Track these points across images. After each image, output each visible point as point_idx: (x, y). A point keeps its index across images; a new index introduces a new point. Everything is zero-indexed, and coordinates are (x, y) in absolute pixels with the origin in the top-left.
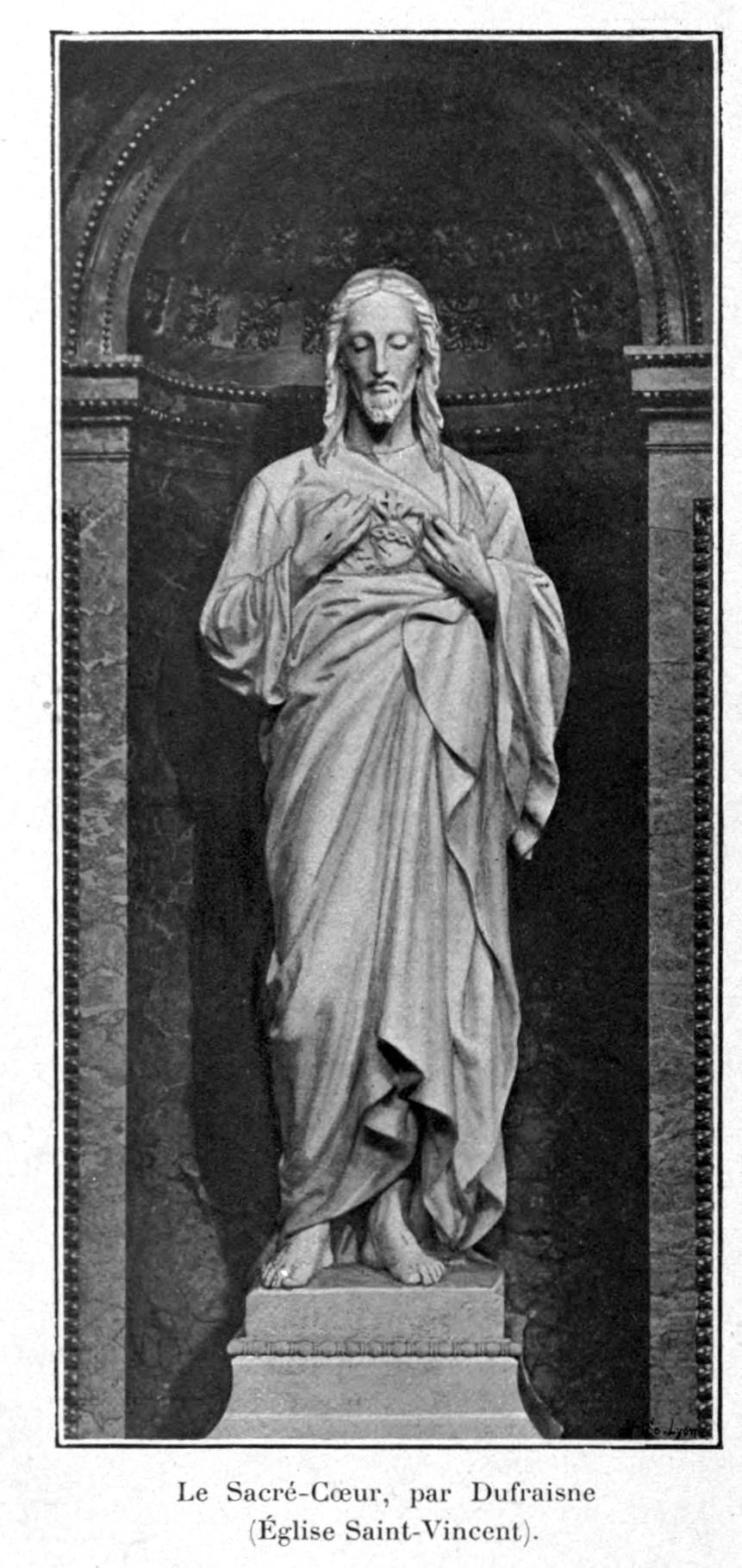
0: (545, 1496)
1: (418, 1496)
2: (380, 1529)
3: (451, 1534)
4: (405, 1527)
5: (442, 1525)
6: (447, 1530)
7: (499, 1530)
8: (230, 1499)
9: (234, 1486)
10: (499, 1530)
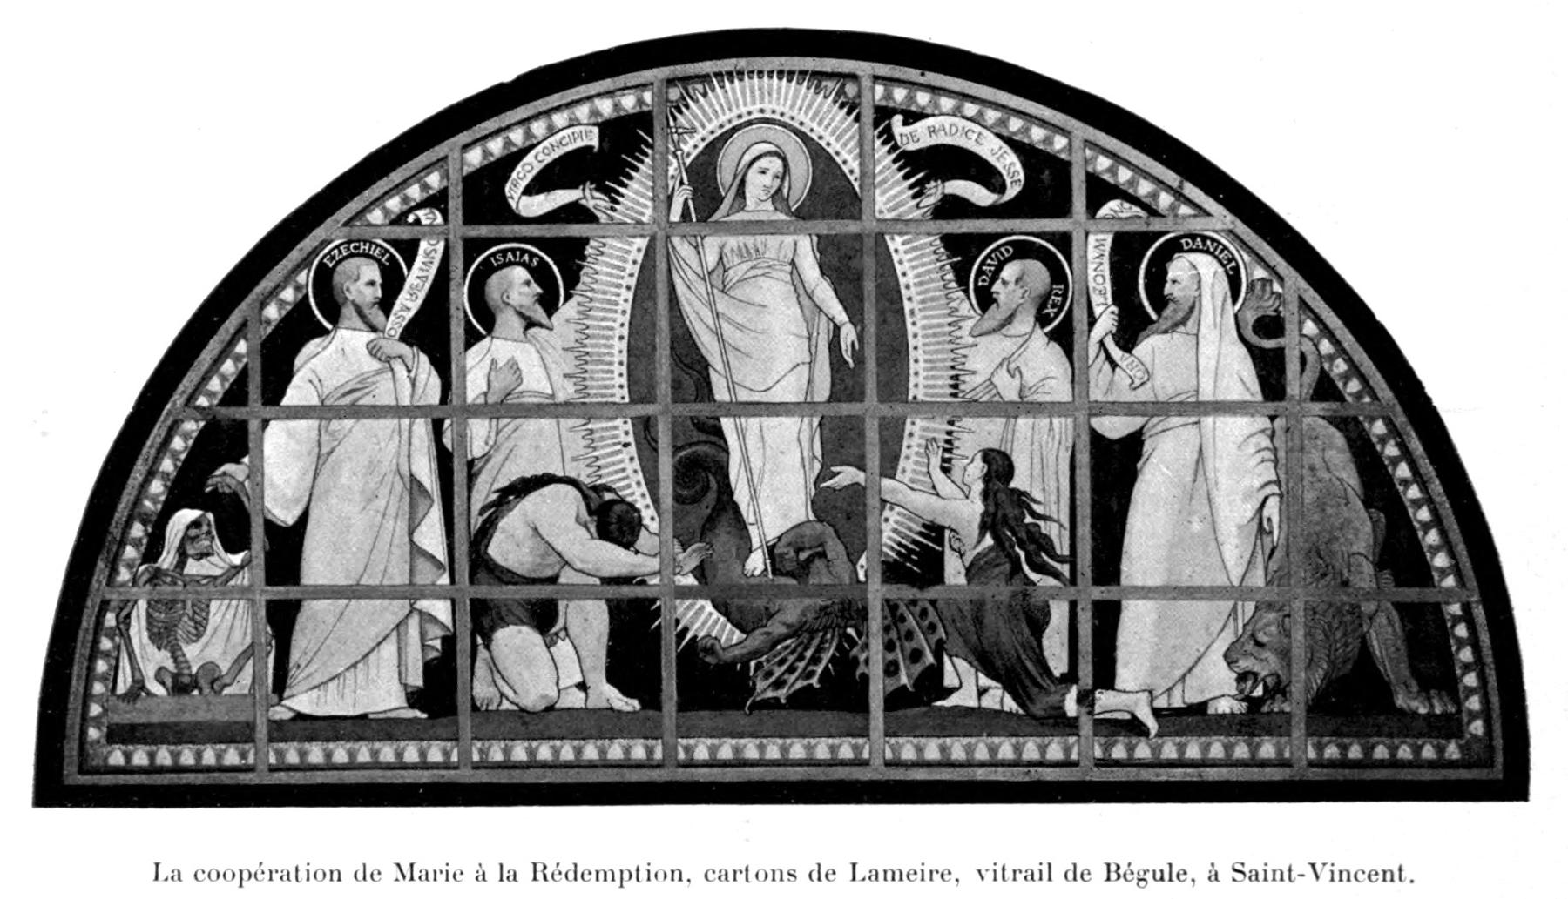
0: (1261, 876)
1: (246, 875)
2: (1265, 871)
3: (1337, 877)
4: (1290, 870)
5: (1328, 867)
6: (1332, 872)
7: (597, 872)
8: (1234, 880)
9: (1239, 867)
10: (1385, 872)
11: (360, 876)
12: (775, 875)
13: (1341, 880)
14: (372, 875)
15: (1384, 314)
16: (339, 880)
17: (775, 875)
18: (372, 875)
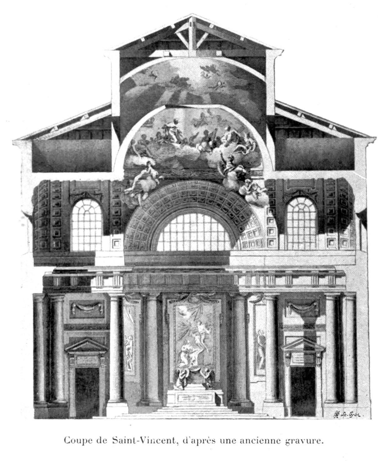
0: (123, 442)
1: (85, 441)
3: (150, 442)
5: (147, 438)
7: (266, 440)
8: (113, 443)
9: (115, 438)
10: (168, 440)
11: (99, 441)
12: (248, 441)
13: (128, 443)
14: (260, 441)
15: (353, 129)
16: (187, 443)
17: (248, 441)
18: (260, 441)
